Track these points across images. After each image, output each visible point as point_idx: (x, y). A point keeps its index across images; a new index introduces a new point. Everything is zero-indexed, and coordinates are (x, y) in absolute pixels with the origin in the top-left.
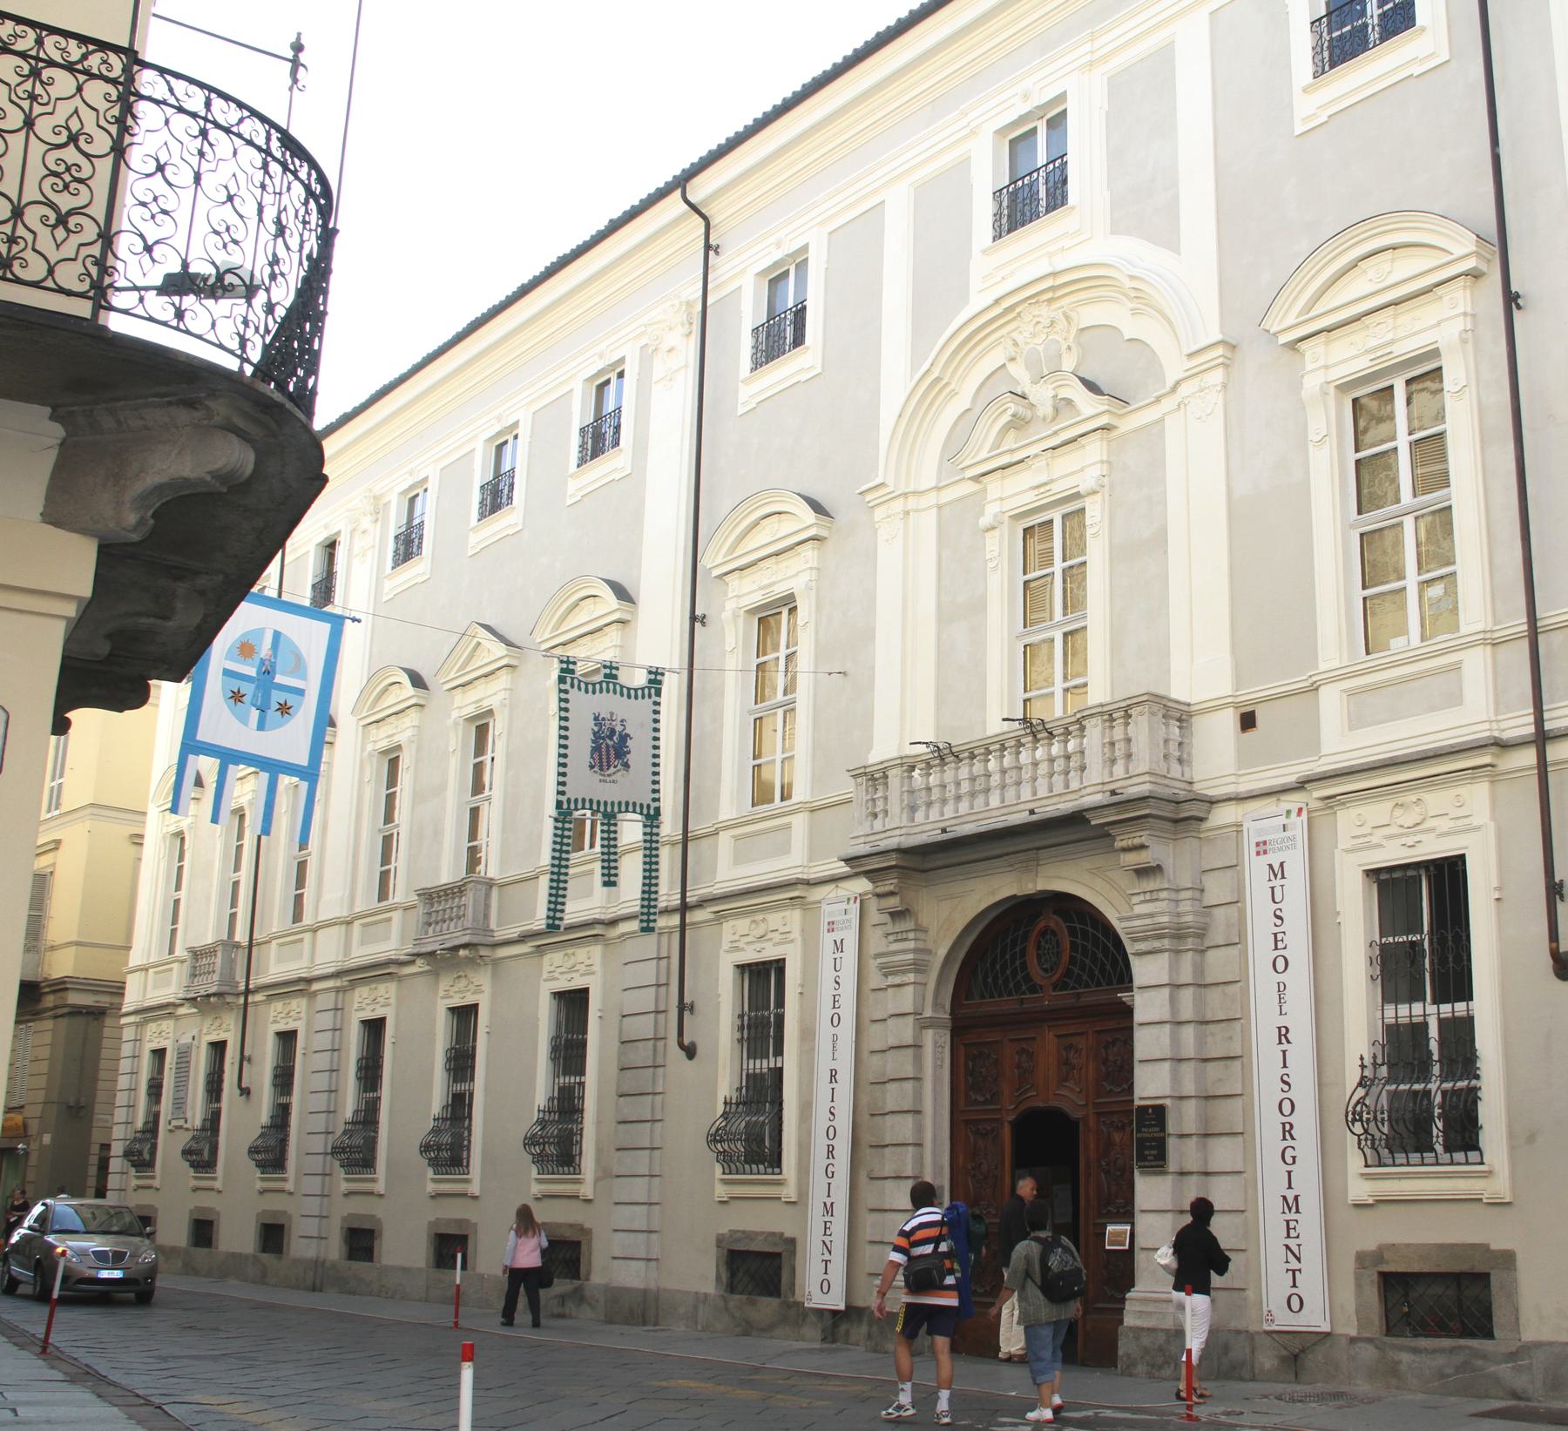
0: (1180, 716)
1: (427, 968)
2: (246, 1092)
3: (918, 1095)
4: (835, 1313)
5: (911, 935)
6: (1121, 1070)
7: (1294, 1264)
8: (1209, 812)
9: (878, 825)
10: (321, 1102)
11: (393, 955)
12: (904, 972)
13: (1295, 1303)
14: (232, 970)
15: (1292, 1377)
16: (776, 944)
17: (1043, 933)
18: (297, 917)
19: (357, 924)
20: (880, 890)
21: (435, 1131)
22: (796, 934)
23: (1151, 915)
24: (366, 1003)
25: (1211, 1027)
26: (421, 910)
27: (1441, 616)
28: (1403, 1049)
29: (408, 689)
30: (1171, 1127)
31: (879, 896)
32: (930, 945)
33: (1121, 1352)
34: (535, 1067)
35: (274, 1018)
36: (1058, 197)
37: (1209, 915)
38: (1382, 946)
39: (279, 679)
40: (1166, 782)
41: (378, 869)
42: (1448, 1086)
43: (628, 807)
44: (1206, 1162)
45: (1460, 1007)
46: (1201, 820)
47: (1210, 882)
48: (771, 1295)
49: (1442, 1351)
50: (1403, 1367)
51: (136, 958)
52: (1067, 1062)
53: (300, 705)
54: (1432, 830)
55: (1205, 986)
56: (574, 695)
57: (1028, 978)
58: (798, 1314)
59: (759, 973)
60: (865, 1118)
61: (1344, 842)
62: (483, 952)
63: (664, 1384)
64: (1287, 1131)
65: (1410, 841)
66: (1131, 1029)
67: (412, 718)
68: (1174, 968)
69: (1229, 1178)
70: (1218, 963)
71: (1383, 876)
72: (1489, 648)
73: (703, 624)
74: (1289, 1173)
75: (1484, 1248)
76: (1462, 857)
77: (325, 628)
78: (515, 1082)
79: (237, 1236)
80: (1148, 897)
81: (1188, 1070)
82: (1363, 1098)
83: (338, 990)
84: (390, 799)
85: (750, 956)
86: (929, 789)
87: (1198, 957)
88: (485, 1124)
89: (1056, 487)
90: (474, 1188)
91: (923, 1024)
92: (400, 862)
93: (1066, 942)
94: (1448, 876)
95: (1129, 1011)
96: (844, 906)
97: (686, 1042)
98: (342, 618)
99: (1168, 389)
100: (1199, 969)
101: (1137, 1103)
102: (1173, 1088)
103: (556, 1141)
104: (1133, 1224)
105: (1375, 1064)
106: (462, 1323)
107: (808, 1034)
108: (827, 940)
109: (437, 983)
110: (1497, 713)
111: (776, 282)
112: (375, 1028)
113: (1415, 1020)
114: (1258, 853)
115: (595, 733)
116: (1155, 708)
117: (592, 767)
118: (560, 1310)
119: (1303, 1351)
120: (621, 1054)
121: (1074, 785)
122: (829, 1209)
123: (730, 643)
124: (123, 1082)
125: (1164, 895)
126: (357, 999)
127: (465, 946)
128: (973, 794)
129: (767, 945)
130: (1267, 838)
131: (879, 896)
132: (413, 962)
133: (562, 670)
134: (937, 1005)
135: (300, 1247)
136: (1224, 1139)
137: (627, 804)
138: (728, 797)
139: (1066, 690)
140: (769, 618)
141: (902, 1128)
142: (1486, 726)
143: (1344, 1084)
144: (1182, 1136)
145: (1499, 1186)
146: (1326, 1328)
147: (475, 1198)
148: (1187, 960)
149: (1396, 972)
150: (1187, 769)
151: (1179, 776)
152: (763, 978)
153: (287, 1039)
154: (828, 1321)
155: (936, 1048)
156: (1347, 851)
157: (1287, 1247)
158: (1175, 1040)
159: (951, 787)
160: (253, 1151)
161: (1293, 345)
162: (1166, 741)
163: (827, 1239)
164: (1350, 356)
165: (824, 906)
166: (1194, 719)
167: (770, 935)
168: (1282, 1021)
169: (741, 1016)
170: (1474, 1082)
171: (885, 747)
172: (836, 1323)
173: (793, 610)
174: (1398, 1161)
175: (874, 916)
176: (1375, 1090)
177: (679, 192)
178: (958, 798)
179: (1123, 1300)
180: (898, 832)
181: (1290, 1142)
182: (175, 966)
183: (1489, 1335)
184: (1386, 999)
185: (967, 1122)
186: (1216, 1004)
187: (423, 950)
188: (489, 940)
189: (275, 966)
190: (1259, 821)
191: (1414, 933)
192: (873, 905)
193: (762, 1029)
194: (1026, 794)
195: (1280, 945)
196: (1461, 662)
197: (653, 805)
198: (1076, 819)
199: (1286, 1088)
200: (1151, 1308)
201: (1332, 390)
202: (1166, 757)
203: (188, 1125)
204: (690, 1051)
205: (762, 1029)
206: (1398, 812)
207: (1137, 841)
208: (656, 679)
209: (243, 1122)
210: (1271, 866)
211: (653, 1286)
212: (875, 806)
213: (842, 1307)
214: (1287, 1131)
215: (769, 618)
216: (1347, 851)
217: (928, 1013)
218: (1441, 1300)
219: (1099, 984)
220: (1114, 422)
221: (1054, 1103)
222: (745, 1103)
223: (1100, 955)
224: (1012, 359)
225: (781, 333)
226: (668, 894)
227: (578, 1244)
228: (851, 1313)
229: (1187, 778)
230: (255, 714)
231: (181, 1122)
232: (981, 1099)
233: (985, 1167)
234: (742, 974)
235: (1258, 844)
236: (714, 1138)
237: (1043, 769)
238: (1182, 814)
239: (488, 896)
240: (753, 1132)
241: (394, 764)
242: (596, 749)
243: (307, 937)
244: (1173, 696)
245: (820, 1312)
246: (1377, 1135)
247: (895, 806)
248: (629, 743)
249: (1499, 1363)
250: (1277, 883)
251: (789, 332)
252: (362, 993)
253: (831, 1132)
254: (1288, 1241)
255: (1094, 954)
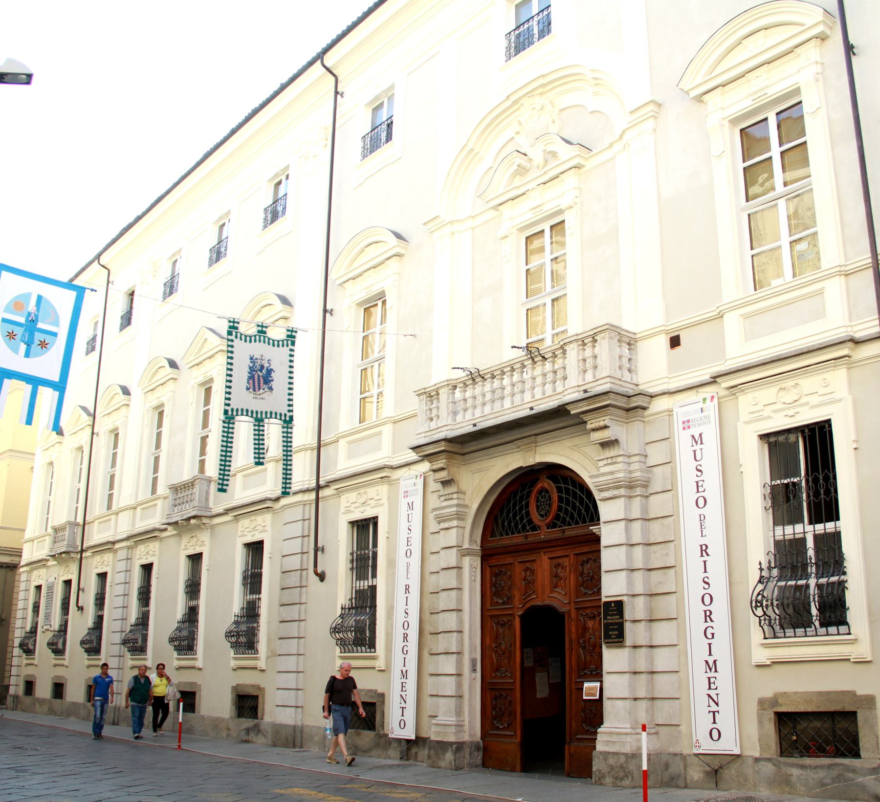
0: (630, 341)
1: (175, 532)
2: (81, 609)
3: (460, 600)
4: (408, 741)
5: (455, 496)
6: (591, 578)
7: (714, 708)
8: (650, 403)
9: (433, 425)
10: (118, 614)
11: (157, 526)
12: (450, 520)
13: (715, 734)
14: (74, 539)
15: (714, 785)
16: (372, 507)
17: (540, 492)
18: (109, 507)
19: (139, 508)
20: (434, 467)
21: (179, 629)
22: (385, 501)
23: (612, 473)
24: (144, 554)
25: (653, 547)
26: (171, 498)
27: (805, 261)
28: (788, 557)
29: (168, 369)
30: (627, 615)
31: (434, 471)
32: (467, 502)
33: (594, 769)
34: (233, 590)
35: (95, 565)
36: (546, 29)
37: (651, 472)
38: (773, 487)
39: (40, 325)
40: (621, 383)
41: (152, 476)
42: (823, 581)
43: (272, 415)
44: (651, 639)
45: (830, 526)
46: (644, 408)
47: (651, 450)
48: (370, 729)
49: (822, 767)
50: (794, 779)
51: (28, 535)
52: (556, 576)
53: (54, 343)
54: (807, 404)
55: (649, 520)
56: (237, 343)
57: (530, 522)
58: (385, 742)
59: (363, 526)
60: (427, 616)
61: (744, 416)
62: (205, 521)
63: (283, 791)
64: (708, 616)
65: (791, 413)
66: (599, 551)
67: (171, 385)
68: (627, 508)
69: (667, 649)
70: (658, 505)
71: (772, 440)
72: (843, 277)
73: (331, 314)
74: (710, 644)
75: (852, 694)
76: (828, 422)
77: (73, 294)
78: (222, 601)
79: (44, 690)
80: (609, 461)
81: (638, 576)
82: (763, 590)
83: (129, 548)
84: (159, 435)
85: (358, 516)
86: (465, 400)
87: (644, 500)
88: (206, 625)
89: (545, 208)
90: (199, 664)
91: (464, 553)
92: (161, 475)
93: (555, 496)
94: (819, 437)
95: (597, 539)
96: (414, 480)
97: (319, 571)
98: (84, 289)
99: (617, 137)
100: (645, 509)
101: (604, 599)
102: (628, 589)
103: (244, 637)
104: (601, 682)
105: (770, 568)
106: (183, 746)
107: (392, 563)
108: (403, 503)
109: (181, 539)
110: (850, 320)
111: (377, 109)
112: (147, 569)
113: (797, 536)
114: (684, 429)
115: (250, 368)
116: (613, 334)
117: (248, 389)
118: (247, 738)
119: (721, 767)
120: (282, 579)
121: (559, 389)
122: (404, 674)
123: (346, 317)
124: (21, 605)
125: (620, 459)
126: (138, 553)
127: (194, 517)
128: (493, 401)
129: (197, 547)
130: (689, 418)
131: (434, 471)
132: (166, 530)
133: (230, 327)
134: (471, 540)
135: (276, 712)
136: (664, 623)
137: (271, 413)
138: (344, 416)
139: (553, 335)
140: (374, 304)
141: (449, 621)
142: (844, 329)
143: (748, 583)
144: (634, 621)
145: (862, 650)
146: (737, 751)
147: (200, 669)
148: (637, 502)
149: (783, 503)
150: (634, 376)
151: (629, 380)
152: (365, 528)
153: (103, 576)
154: (404, 745)
155: (472, 567)
156: (747, 423)
157: (709, 696)
158: (629, 557)
159: (479, 398)
160: (83, 643)
161: (699, 99)
162: (620, 357)
163: (403, 694)
164: (740, 100)
165: (402, 482)
166: (639, 344)
167: (369, 502)
168: (703, 541)
169: (352, 554)
170: (843, 577)
171: (441, 372)
172: (410, 747)
173: (384, 302)
174: (787, 635)
175: (434, 486)
176: (771, 585)
177: (319, 61)
178: (484, 404)
179: (596, 733)
180: (445, 428)
181: (710, 624)
182: (47, 538)
183: (857, 755)
184: (775, 523)
185: (492, 617)
186: (657, 532)
187: (171, 521)
188: (208, 514)
189: (96, 536)
190: (684, 407)
191: (795, 477)
192: (432, 476)
193: (364, 563)
194: (528, 397)
195: (701, 489)
196: (823, 289)
197: (289, 414)
198: (560, 413)
199: (706, 586)
200: (614, 738)
201: (726, 123)
202: (620, 368)
203: (52, 629)
204: (322, 577)
205: (364, 563)
206: (781, 393)
207: (602, 424)
208: (291, 336)
209: (80, 625)
210: (693, 436)
211: (299, 723)
212: (431, 413)
213: (413, 737)
214: (708, 616)
215: (374, 304)
216: (747, 423)
217: (466, 545)
218: (815, 732)
219: (577, 523)
220: (582, 162)
221: (547, 602)
222: (356, 608)
223: (578, 504)
224: (518, 133)
225: (380, 134)
226: (303, 476)
227: (257, 697)
228: (419, 741)
229: (635, 381)
230: (23, 347)
231: (48, 627)
232: (500, 601)
233: (503, 646)
234: (353, 527)
235: (684, 423)
236: (335, 630)
237: (539, 380)
238: (631, 405)
239: (209, 487)
240: (359, 627)
241: (161, 414)
242: (251, 378)
243: (113, 517)
244: (624, 327)
245: (399, 740)
246: (773, 616)
247: (443, 412)
248: (273, 374)
249: (864, 775)
250: (697, 447)
251: (384, 135)
252: (142, 548)
253: (406, 625)
254: (710, 692)
255: (574, 503)
